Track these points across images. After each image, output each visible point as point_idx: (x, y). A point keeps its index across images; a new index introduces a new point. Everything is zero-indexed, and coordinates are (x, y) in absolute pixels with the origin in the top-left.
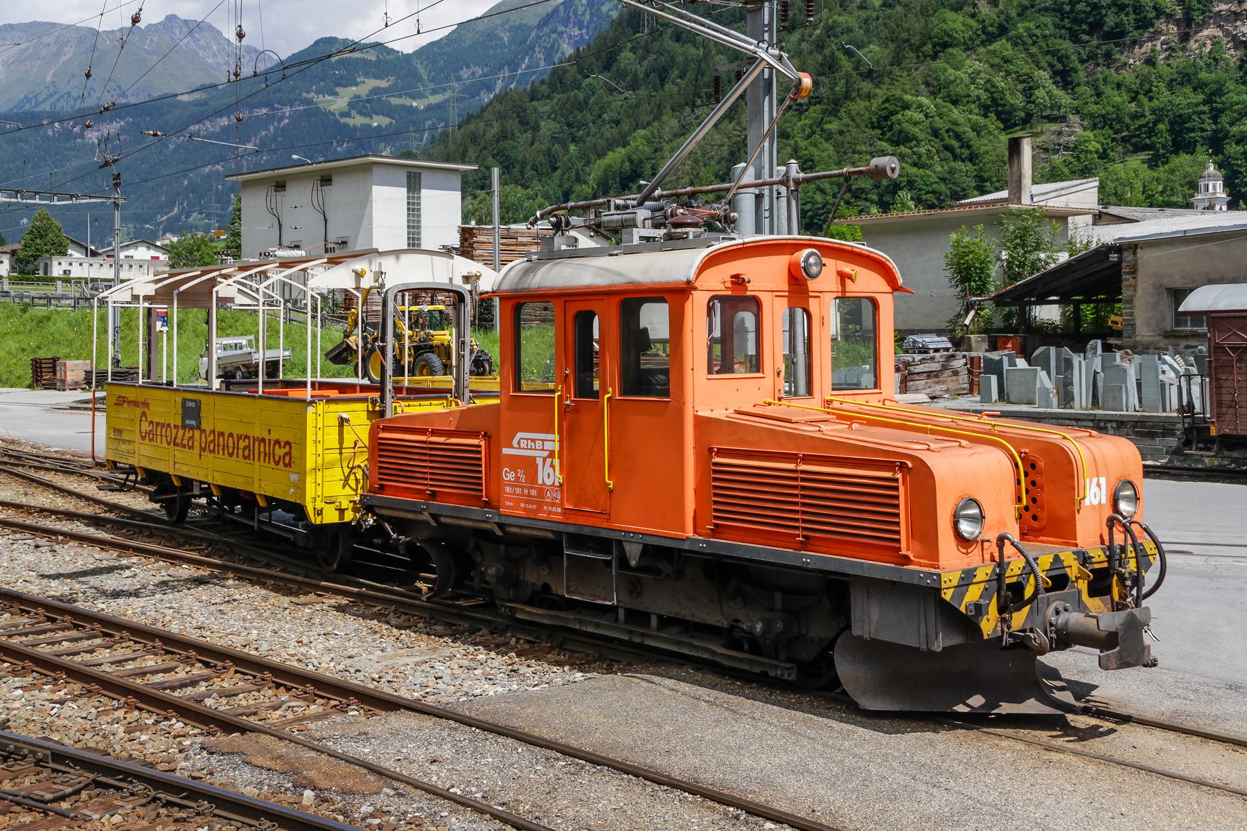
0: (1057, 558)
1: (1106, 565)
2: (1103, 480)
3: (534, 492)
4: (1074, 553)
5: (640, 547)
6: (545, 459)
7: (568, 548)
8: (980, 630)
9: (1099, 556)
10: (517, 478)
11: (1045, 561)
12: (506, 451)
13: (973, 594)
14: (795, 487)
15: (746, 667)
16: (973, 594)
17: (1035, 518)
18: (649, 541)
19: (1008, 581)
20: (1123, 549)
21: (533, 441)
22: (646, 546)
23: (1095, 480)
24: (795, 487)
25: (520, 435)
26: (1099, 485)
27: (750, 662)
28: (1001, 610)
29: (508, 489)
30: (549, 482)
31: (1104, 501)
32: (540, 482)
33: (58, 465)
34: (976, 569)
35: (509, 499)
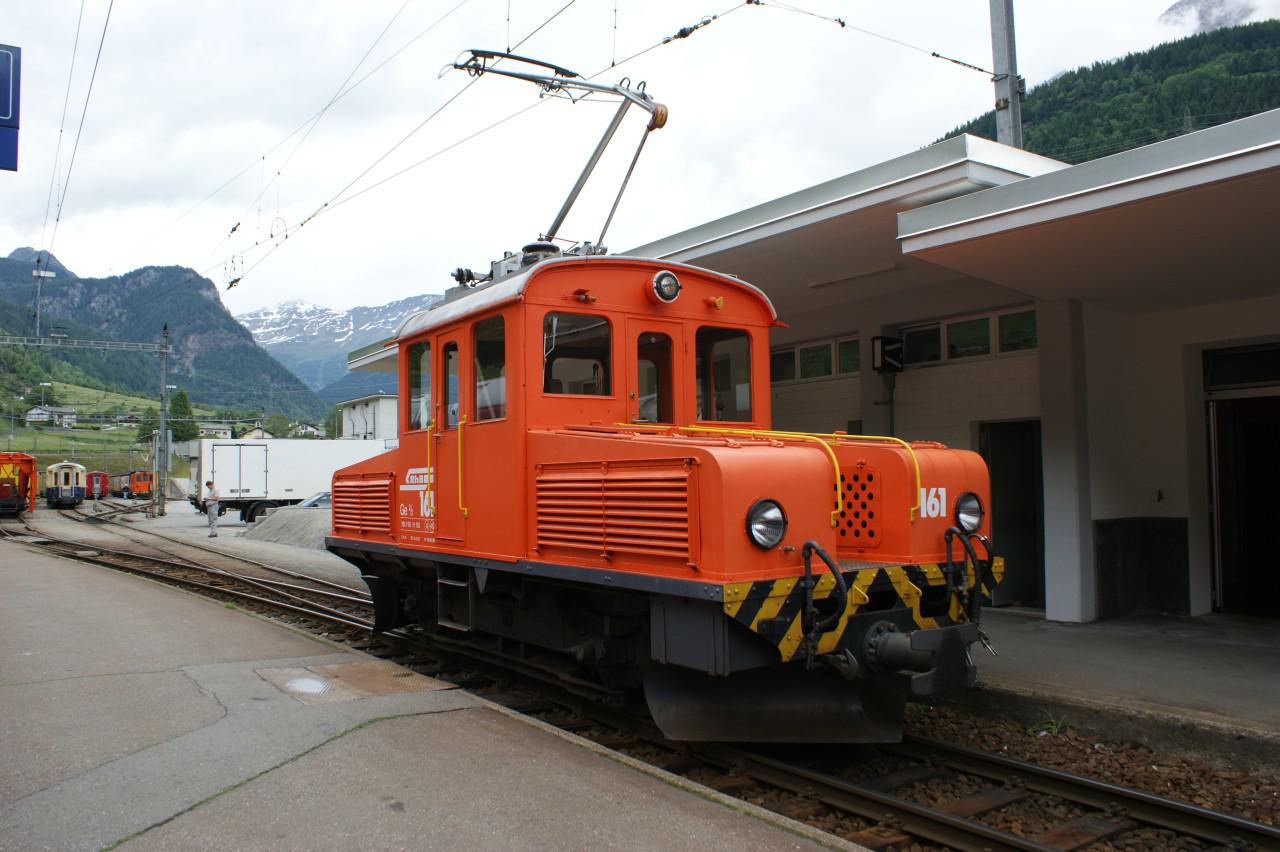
0: (882, 573)
1: (943, 582)
2: (942, 491)
3: (418, 525)
4: (904, 568)
5: (487, 572)
6: (425, 492)
7: (442, 577)
8: (779, 653)
9: (933, 572)
10: (409, 512)
11: (867, 576)
12: (403, 488)
13: (769, 610)
14: (357, 509)
15: (583, 694)
16: (769, 610)
17: (871, 534)
18: (493, 567)
19: (816, 596)
20: (963, 565)
21: (418, 475)
22: (491, 572)
23: (933, 490)
24: (357, 509)
25: (411, 471)
26: (937, 496)
27: (582, 687)
28: (807, 629)
29: (403, 523)
30: (427, 516)
31: (943, 514)
32: (422, 515)
33: (205, 582)
34: (773, 582)
35: (404, 533)
